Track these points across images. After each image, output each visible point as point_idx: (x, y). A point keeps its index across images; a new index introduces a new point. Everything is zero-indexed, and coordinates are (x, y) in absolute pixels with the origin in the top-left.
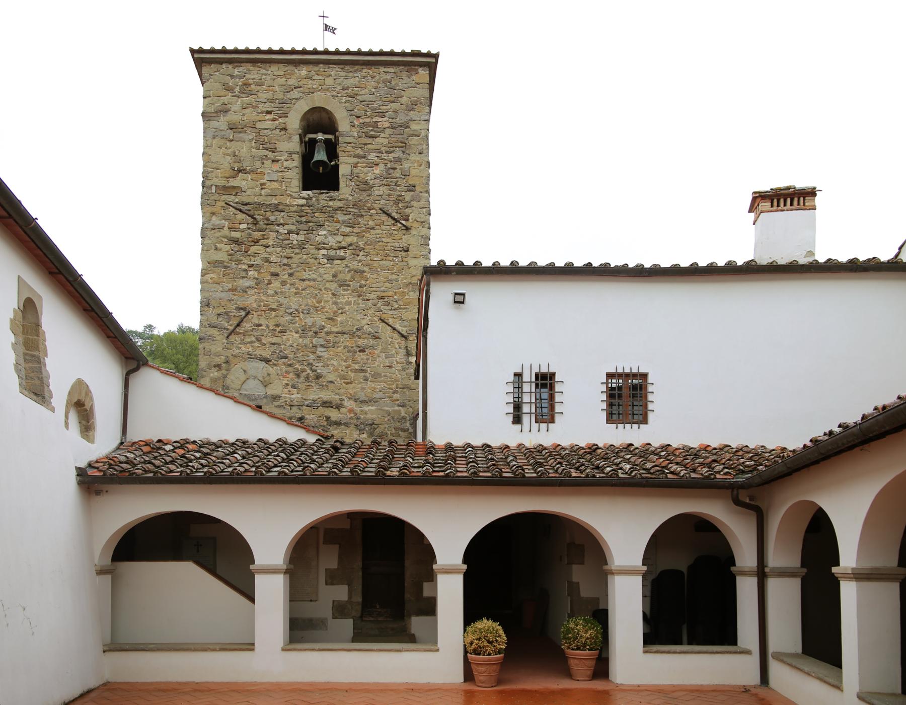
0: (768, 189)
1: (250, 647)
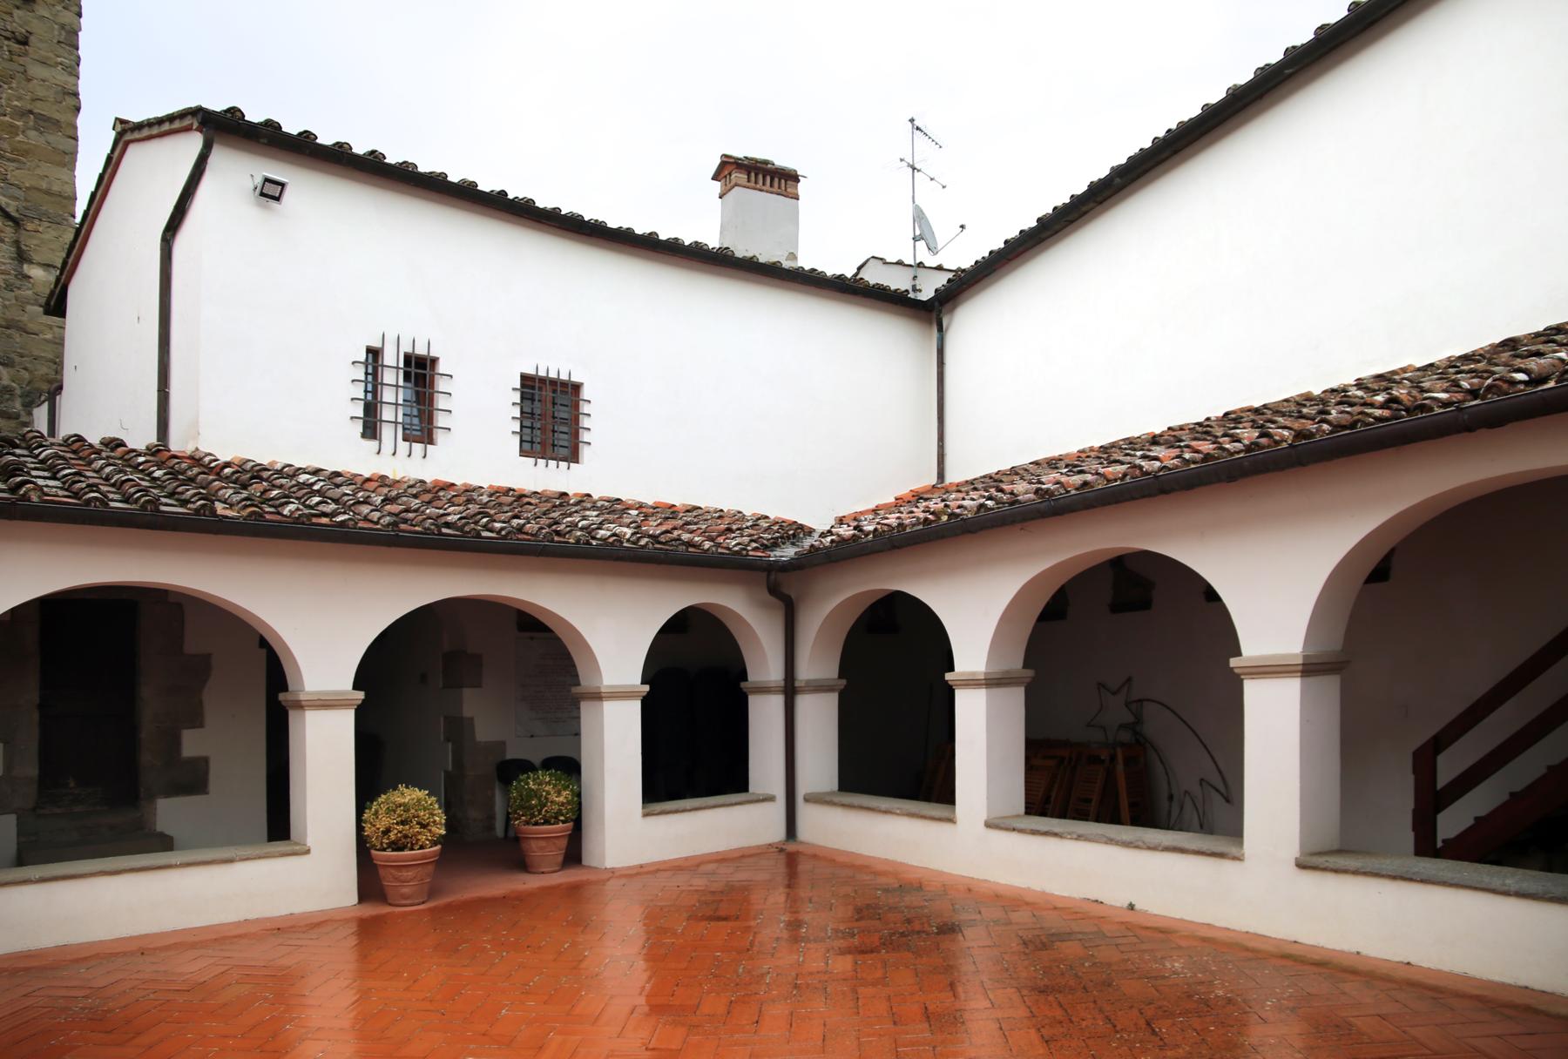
0: (741, 156)
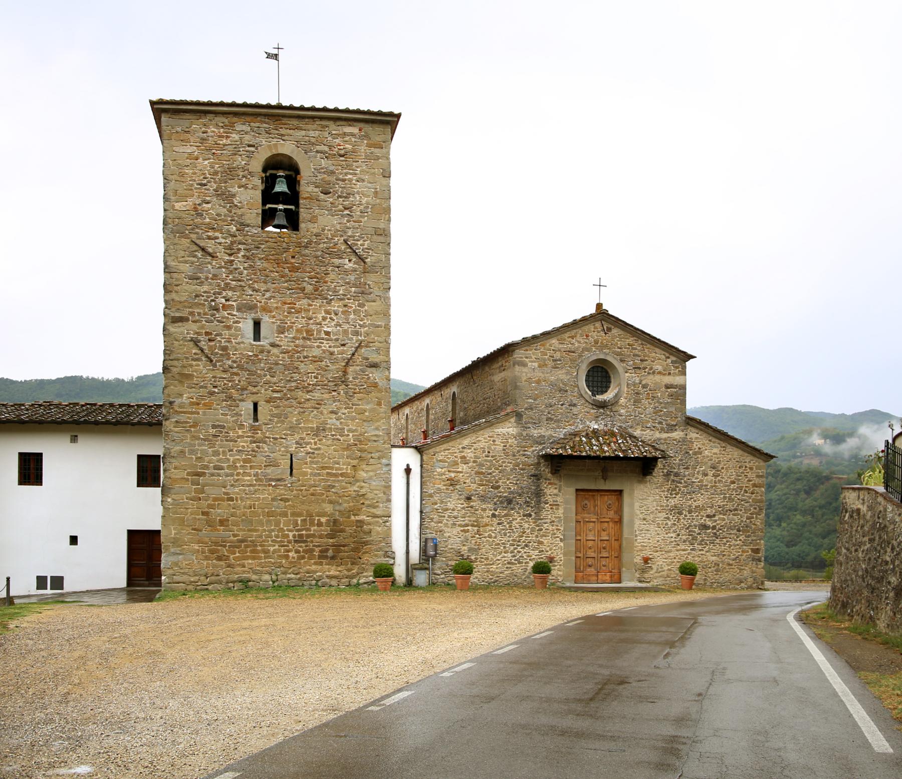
1: (577, 490)
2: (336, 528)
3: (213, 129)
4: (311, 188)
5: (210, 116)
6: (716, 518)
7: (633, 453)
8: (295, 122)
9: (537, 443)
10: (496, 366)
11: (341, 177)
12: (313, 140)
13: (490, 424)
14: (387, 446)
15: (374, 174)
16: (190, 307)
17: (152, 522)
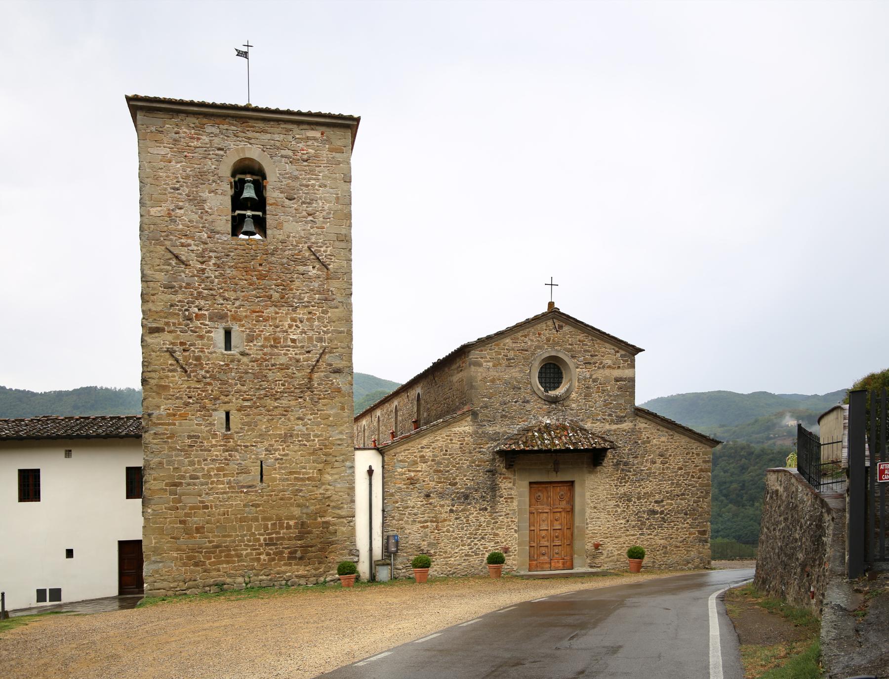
1: (531, 483)
2: (303, 530)
3: (185, 129)
4: (276, 194)
5: (182, 116)
6: (664, 503)
7: (582, 445)
8: (261, 125)
9: (492, 440)
10: (454, 367)
11: (304, 182)
12: (278, 144)
13: (447, 424)
14: (350, 449)
15: (336, 178)
16: (166, 318)
17: (135, 533)
